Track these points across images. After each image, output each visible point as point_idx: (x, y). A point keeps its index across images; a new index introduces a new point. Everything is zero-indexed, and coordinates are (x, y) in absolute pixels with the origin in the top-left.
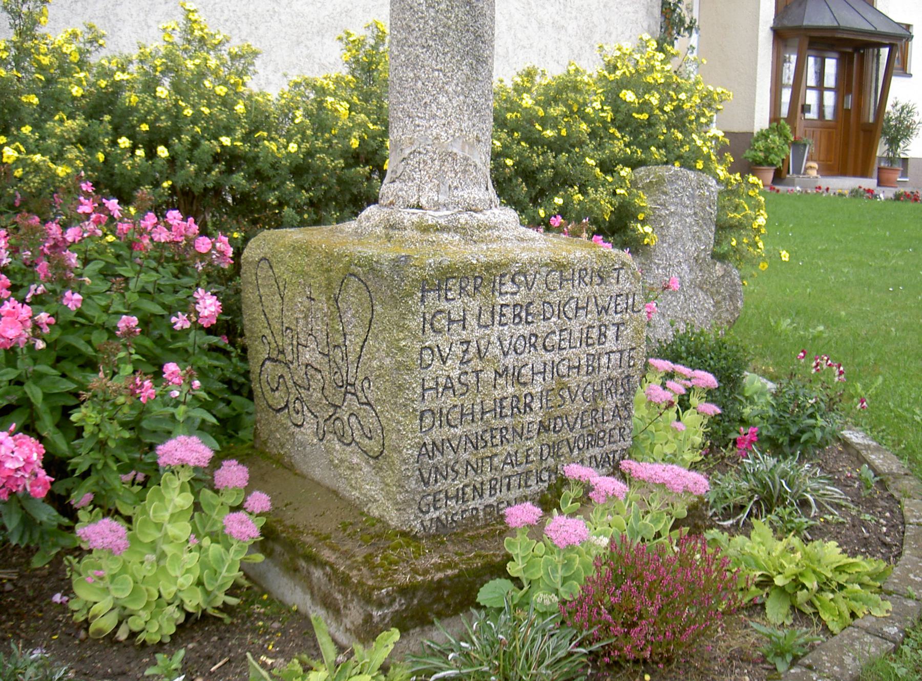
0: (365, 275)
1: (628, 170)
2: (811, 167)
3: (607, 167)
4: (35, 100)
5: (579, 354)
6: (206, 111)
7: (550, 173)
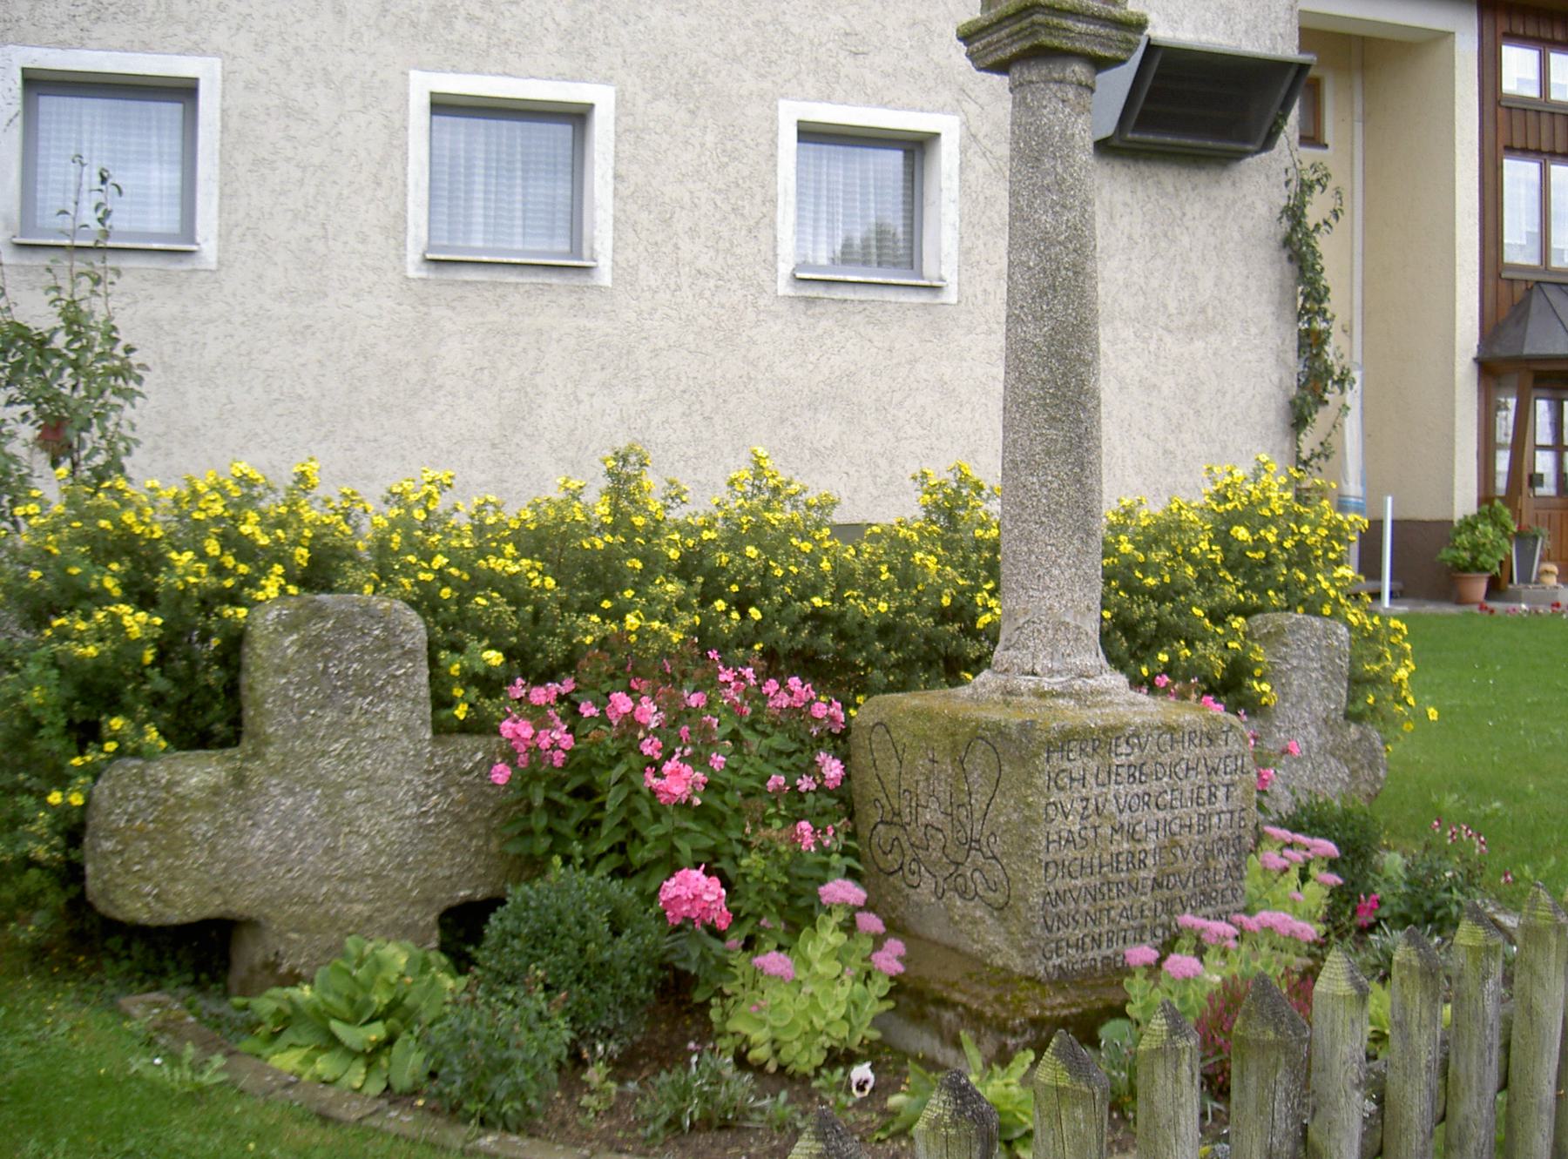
0: (969, 740)
1: (1241, 619)
2: (1547, 572)
3: (1217, 617)
4: (639, 565)
5: (1191, 813)
6: (795, 570)
7: (1153, 625)
